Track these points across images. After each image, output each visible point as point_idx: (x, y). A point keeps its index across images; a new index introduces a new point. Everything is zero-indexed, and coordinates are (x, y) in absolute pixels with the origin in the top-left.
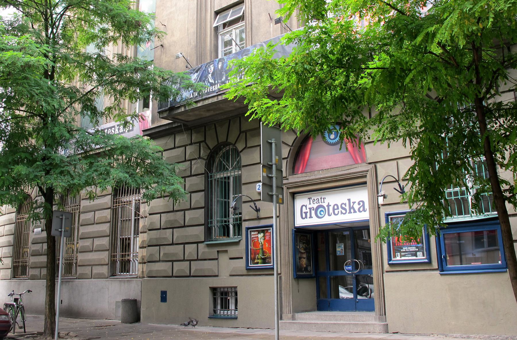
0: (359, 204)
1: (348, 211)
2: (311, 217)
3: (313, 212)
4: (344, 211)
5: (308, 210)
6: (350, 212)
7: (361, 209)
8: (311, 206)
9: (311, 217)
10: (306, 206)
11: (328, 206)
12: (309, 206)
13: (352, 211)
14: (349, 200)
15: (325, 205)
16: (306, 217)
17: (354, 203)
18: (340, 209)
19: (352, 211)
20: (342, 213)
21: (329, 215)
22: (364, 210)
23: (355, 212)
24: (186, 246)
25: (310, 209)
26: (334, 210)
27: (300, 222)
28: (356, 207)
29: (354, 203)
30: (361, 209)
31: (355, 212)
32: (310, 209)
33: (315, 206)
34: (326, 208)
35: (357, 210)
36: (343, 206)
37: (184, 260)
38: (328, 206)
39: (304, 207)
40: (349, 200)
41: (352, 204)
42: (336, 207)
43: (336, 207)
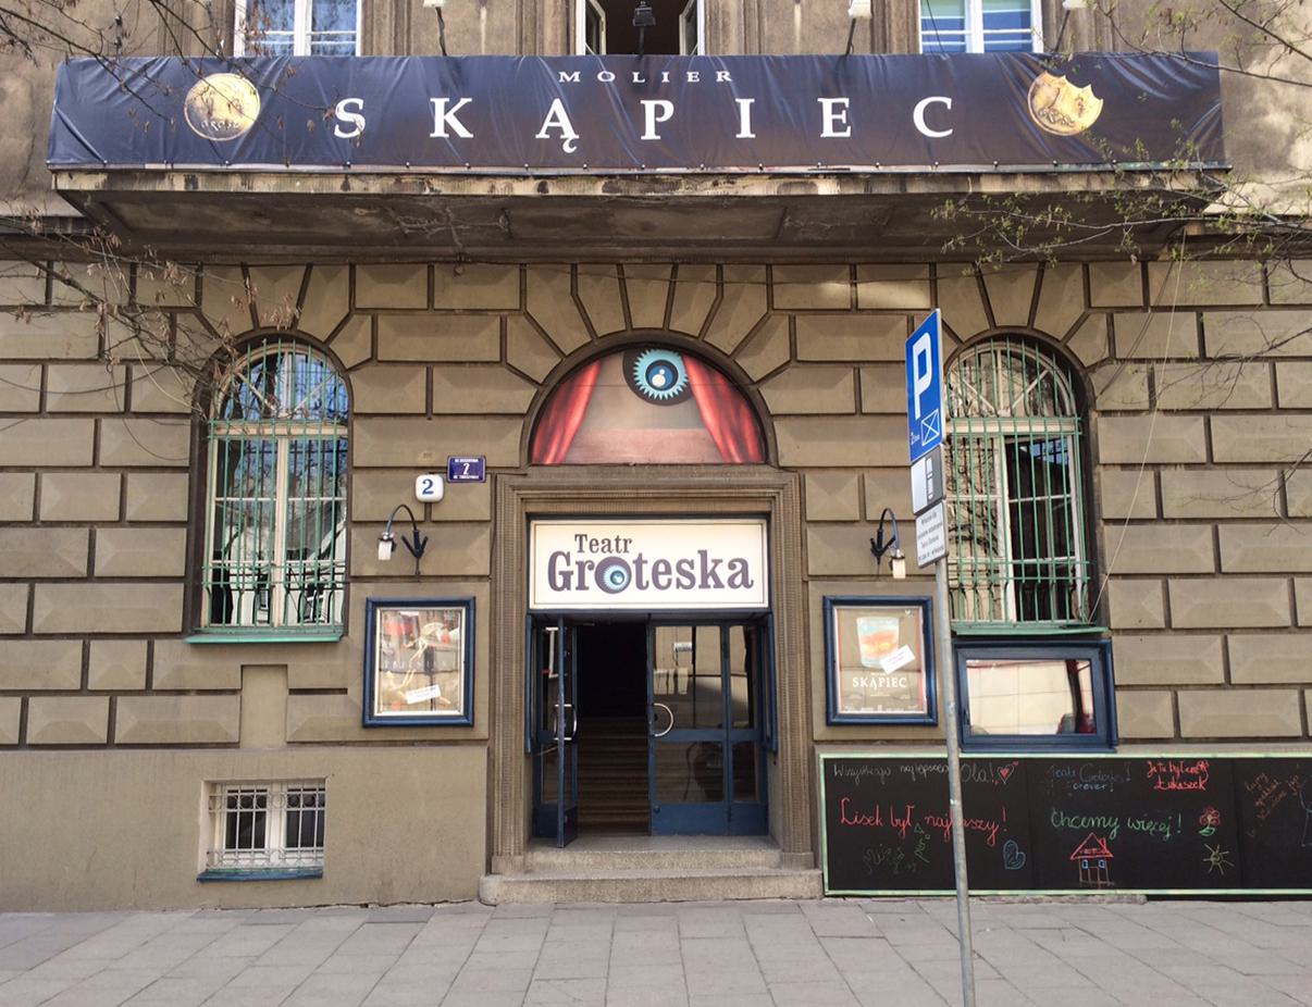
0: (732, 566)
1: (698, 581)
2: (582, 586)
3: (590, 576)
4: (686, 582)
5: (574, 568)
6: (704, 585)
7: (738, 580)
8: (584, 557)
9: (582, 586)
10: (567, 557)
11: (640, 562)
12: (575, 557)
13: (711, 581)
14: (703, 554)
15: (629, 558)
16: (567, 585)
17: (717, 562)
18: (675, 575)
19: (711, 581)
20: (679, 584)
21: (640, 586)
22: (746, 583)
23: (719, 585)
24: (95, 645)
25: (581, 565)
26: (655, 573)
27: (544, 597)
28: (724, 573)
29: (717, 562)
30: (738, 580)
31: (719, 585)
32: (581, 565)
33: (598, 558)
34: (633, 568)
35: (724, 581)
36: (685, 566)
37: (83, 690)
38: (640, 562)
39: (561, 561)
40: (703, 554)
41: (710, 565)
42: (662, 568)
43: (662, 568)
